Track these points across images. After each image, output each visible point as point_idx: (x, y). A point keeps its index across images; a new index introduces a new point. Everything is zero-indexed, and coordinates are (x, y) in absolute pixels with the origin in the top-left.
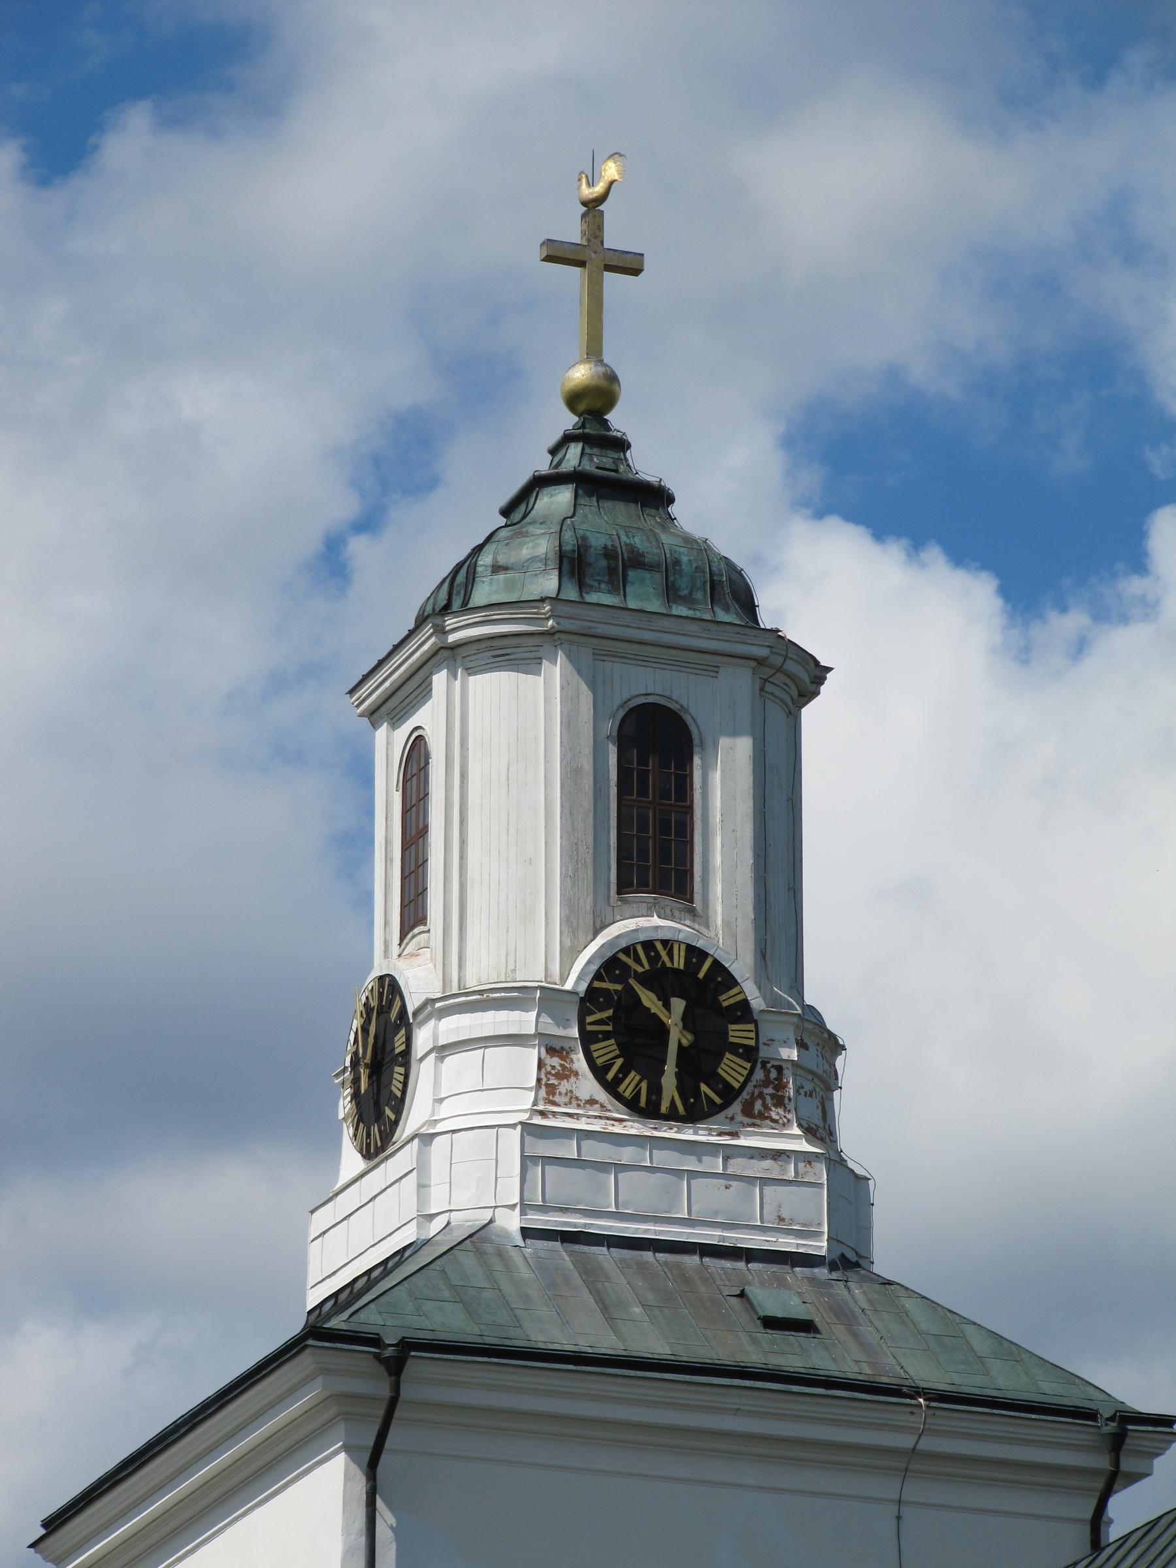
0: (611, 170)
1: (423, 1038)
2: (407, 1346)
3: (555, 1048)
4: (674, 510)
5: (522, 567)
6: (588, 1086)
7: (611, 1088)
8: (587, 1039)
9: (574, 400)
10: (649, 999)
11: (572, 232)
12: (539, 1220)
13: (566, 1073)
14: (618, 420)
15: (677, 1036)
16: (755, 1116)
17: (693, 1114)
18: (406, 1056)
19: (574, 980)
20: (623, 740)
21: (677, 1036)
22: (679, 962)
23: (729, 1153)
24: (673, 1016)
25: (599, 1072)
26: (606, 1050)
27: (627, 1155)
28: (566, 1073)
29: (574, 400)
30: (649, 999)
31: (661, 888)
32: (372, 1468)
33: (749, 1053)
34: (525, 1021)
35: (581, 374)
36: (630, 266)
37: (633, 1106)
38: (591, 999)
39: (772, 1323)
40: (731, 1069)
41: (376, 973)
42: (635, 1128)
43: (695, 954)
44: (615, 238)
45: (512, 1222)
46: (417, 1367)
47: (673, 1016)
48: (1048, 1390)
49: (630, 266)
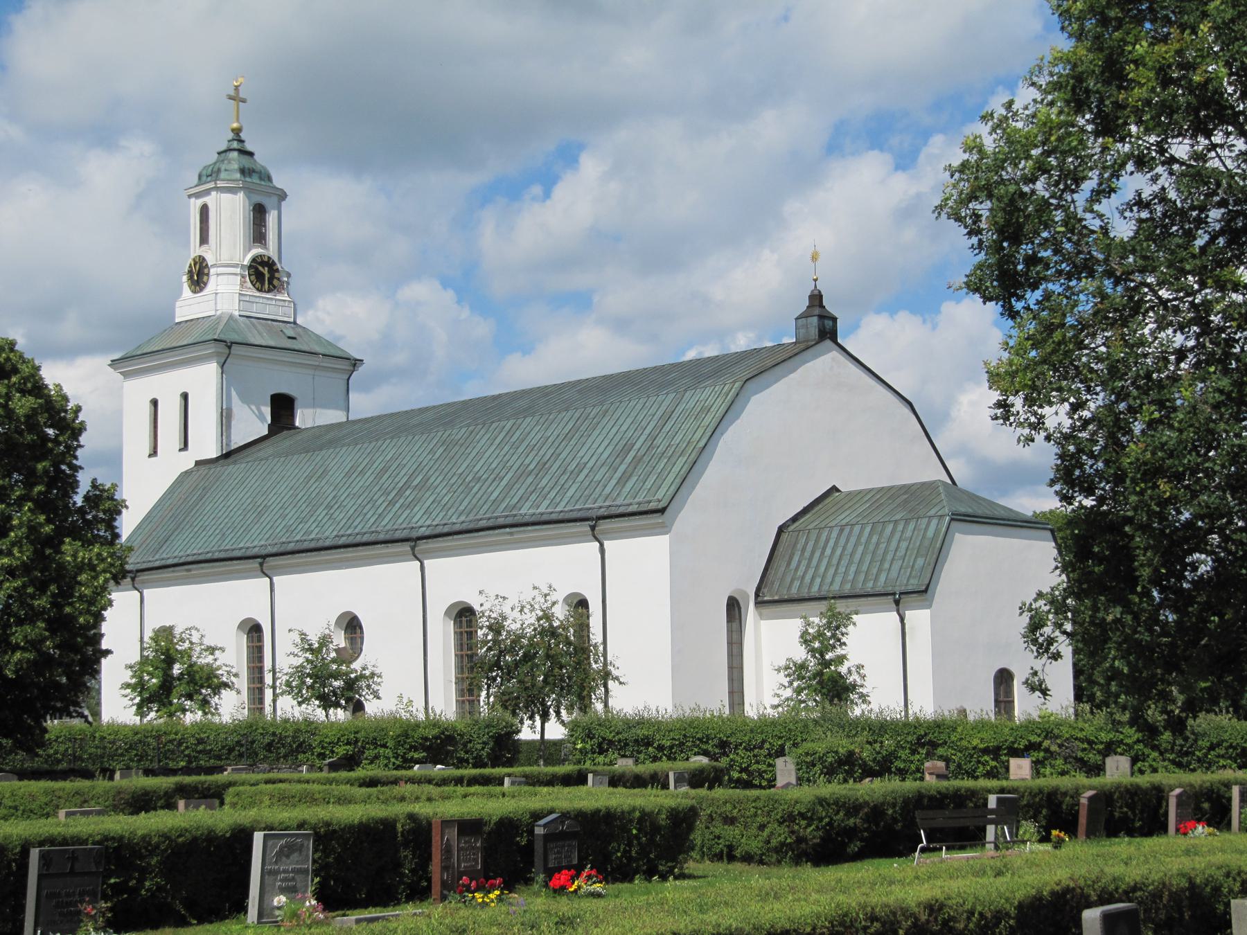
0: (241, 80)
1: (212, 271)
2: (232, 343)
3: (243, 277)
4: (255, 157)
5: (231, 171)
6: (249, 284)
7: (254, 285)
8: (250, 275)
9: (233, 130)
10: (261, 268)
11: (232, 93)
12: (242, 313)
13: (245, 282)
14: (243, 135)
15: (267, 276)
16: (279, 292)
17: (269, 291)
18: (208, 275)
19: (246, 262)
20: (254, 209)
21: (267, 276)
22: (266, 259)
23: (276, 300)
24: (265, 271)
25: (252, 282)
26: (253, 277)
27: (257, 300)
28: (245, 282)
29: (233, 130)
30: (261, 268)
31: (260, 243)
32: (222, 367)
33: (278, 279)
34: (238, 270)
35: (235, 125)
36: (244, 101)
37: (258, 289)
38: (250, 267)
39: (289, 338)
40: (275, 282)
41: (193, 255)
42: (258, 294)
43: (269, 258)
44: (242, 95)
45: (237, 313)
46: (234, 347)
47: (265, 271)
48: (339, 354)
49: (244, 101)
